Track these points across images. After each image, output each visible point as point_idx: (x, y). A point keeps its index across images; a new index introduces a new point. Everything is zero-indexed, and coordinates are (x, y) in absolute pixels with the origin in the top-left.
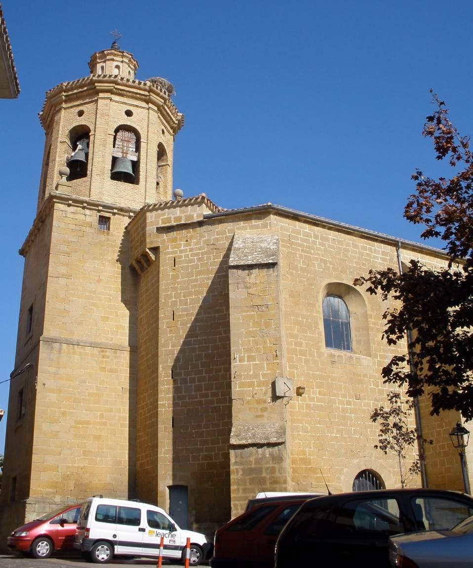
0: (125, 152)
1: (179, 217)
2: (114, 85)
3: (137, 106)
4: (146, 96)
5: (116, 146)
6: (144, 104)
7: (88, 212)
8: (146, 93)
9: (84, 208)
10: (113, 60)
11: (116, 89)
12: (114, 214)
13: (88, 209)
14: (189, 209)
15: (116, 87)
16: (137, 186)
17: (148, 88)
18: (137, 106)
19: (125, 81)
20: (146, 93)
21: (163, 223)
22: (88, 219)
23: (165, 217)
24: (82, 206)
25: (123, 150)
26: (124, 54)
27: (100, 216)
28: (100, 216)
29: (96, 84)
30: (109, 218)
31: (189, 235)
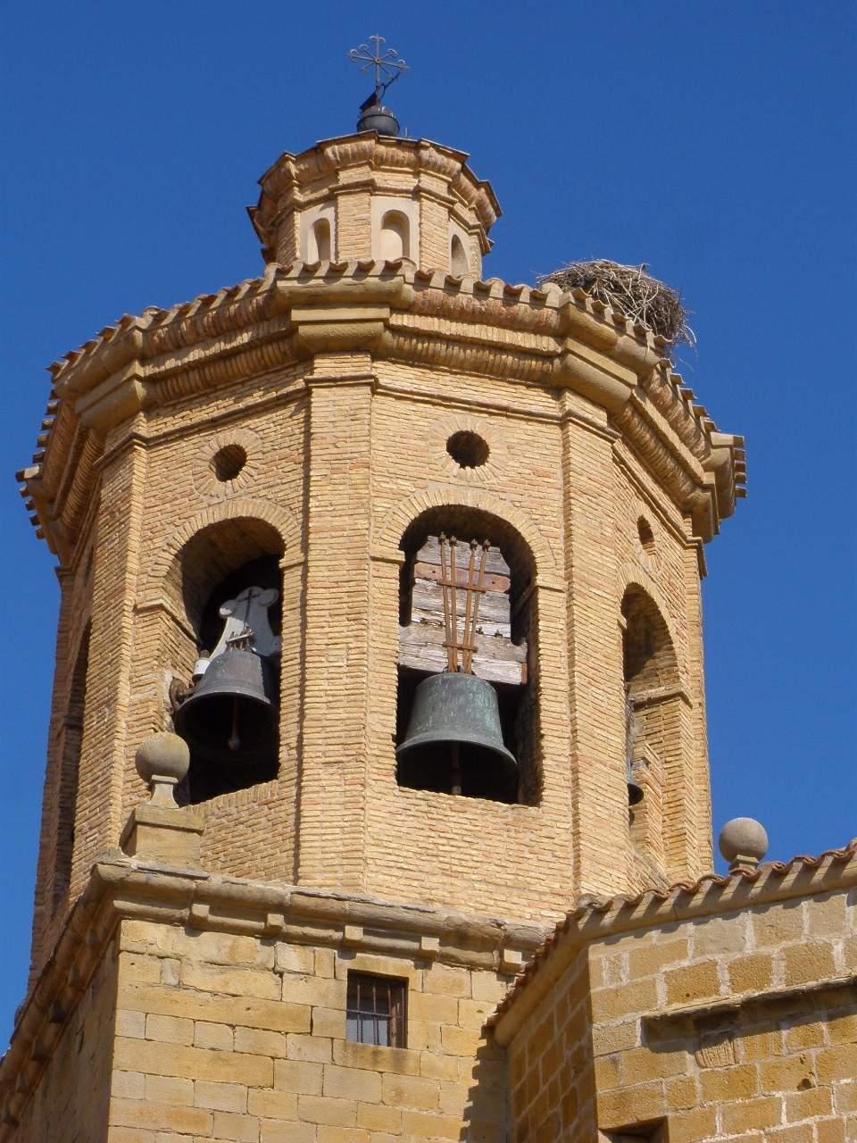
0: (460, 641)
1: (752, 960)
2: (384, 312)
3: (505, 411)
4: (548, 357)
5: (416, 616)
6: (538, 401)
7: (290, 956)
8: (548, 344)
9: (270, 936)
10: (369, 187)
11: (397, 331)
12: (424, 960)
13: (289, 939)
14: (806, 917)
15: (398, 320)
16: (532, 810)
17: (554, 319)
18: (505, 411)
19: (435, 292)
20: (548, 344)
21: (674, 995)
22: (297, 993)
23: (686, 963)
24: (259, 925)
25: (451, 635)
26: (425, 154)
27: (354, 976)
28: (354, 976)
29: (297, 315)
30: (400, 984)
31: (814, 1053)
